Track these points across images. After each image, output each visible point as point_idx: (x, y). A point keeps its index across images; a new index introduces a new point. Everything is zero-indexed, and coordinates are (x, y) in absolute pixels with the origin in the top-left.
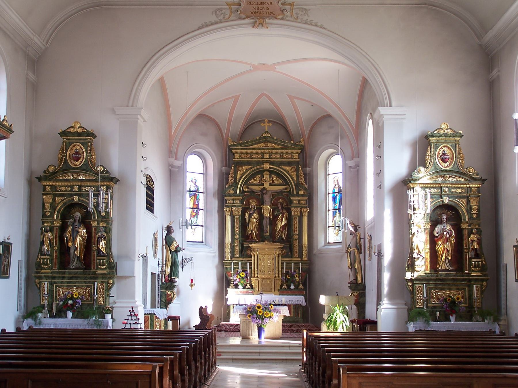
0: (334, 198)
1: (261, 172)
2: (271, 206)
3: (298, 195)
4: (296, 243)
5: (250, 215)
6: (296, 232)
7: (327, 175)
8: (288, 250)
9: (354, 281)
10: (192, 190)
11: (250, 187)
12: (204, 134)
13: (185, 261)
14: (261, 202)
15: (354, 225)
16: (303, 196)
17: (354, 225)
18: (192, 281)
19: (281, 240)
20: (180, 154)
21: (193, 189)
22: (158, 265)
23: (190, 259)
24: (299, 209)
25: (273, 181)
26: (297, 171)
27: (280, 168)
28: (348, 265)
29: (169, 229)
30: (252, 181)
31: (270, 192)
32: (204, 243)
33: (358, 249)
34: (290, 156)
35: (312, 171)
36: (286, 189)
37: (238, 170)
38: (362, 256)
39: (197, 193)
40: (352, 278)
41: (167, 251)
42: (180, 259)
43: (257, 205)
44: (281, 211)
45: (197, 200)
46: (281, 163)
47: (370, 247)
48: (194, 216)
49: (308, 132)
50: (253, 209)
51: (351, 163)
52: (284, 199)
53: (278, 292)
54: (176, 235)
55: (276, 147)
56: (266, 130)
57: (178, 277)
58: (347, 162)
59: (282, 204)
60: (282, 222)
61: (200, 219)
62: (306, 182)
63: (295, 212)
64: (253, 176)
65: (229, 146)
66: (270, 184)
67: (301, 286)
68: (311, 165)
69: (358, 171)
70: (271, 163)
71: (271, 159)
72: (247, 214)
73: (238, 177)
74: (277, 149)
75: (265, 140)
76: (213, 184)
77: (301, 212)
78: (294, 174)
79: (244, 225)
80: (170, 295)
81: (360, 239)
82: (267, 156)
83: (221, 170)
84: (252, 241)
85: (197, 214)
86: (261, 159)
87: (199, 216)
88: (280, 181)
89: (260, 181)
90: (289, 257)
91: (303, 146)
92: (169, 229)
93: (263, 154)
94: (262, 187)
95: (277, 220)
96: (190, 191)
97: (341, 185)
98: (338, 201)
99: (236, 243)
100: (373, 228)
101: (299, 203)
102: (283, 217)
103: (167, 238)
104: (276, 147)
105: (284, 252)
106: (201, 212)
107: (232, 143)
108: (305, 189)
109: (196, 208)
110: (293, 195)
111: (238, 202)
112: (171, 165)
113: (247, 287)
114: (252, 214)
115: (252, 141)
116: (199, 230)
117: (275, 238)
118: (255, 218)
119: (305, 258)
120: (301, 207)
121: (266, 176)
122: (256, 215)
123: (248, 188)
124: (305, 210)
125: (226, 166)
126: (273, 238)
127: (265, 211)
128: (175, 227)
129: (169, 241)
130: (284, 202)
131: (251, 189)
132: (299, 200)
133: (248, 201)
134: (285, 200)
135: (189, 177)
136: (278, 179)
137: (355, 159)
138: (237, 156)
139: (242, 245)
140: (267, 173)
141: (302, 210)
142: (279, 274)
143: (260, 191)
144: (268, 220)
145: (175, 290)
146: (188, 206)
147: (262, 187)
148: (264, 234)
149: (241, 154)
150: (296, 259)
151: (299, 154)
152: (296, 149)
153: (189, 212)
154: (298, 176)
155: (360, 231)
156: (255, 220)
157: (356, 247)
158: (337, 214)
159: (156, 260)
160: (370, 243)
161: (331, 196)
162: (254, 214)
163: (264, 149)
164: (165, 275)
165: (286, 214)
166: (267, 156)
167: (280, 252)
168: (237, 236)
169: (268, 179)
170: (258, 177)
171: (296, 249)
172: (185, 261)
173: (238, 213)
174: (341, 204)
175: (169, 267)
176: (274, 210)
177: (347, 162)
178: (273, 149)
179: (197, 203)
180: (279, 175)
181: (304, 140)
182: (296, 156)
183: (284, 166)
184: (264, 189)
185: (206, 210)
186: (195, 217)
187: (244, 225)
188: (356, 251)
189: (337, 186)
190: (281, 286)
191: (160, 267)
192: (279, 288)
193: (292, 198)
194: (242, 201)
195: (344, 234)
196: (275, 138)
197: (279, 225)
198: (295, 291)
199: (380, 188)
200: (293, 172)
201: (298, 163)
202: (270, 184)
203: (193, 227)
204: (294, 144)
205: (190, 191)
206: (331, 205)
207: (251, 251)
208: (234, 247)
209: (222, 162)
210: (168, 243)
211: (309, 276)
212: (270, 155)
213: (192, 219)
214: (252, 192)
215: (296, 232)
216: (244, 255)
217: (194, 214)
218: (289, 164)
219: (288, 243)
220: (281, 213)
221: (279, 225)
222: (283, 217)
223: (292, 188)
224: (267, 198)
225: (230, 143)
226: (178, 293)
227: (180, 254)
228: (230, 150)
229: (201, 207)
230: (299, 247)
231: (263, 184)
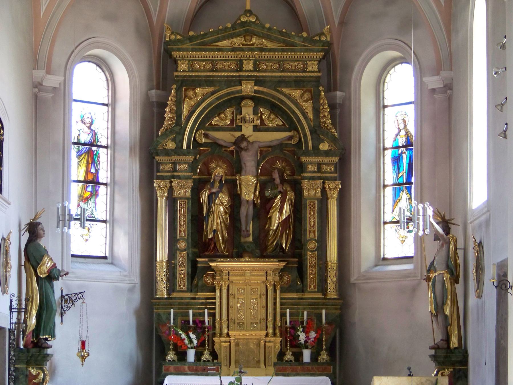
0: (397, 160)
1: (236, 102)
2: (257, 176)
3: (316, 151)
4: (311, 259)
5: (212, 197)
6: (312, 235)
7: (380, 107)
8: (295, 273)
9: (444, 345)
10: (82, 141)
11: (212, 134)
12: (111, 17)
13: (69, 300)
14: (236, 168)
15: (443, 218)
16: (327, 153)
17: (443, 218)
18: (83, 343)
19: (278, 253)
20: (58, 60)
21: (85, 138)
22: (11, 308)
23: (80, 296)
24: (319, 183)
25: (262, 121)
26: (315, 98)
27: (278, 91)
28: (430, 308)
29: (34, 230)
30: (215, 121)
31: (256, 146)
32: (109, 261)
33: (451, 273)
34: (300, 66)
35: (347, 99)
36: (291, 138)
37: (186, 96)
38: (459, 288)
39: (94, 148)
40: (439, 337)
41: (29, 277)
42: (57, 295)
43: (226, 175)
44: (280, 189)
45: (93, 162)
46: (279, 82)
47: (480, 269)
48: (87, 199)
49: (340, 11)
50: (217, 184)
51: (433, 82)
52: (286, 161)
53: (272, 369)
54: (48, 242)
55: (270, 45)
56: (248, 7)
57: (54, 336)
58: (424, 79)
59: (281, 173)
60: (280, 214)
61: (101, 207)
62: (334, 124)
63: (311, 190)
64: (217, 110)
65: (167, 43)
66: (256, 129)
67: (324, 356)
68: (345, 86)
69: (450, 99)
70: (258, 82)
71: (259, 71)
72: (205, 196)
73: (185, 112)
74: (270, 50)
75: (246, 30)
76: (127, 124)
77: (324, 190)
78: (308, 106)
79: (198, 219)
80: (36, 377)
81: (456, 249)
82: (249, 66)
83: (147, 97)
84: (217, 256)
85: (95, 194)
86: (237, 71)
87: (98, 200)
88: (278, 122)
89: (233, 121)
90: (297, 291)
91: (329, 44)
92: (34, 230)
93: (241, 61)
94: (238, 134)
95: (271, 207)
96: (78, 143)
97: (412, 128)
98: (405, 166)
99: (181, 258)
100: (487, 223)
101: (319, 170)
102: (283, 202)
103: (31, 249)
104: (270, 45)
105: (285, 279)
106: (102, 190)
107: (173, 37)
108: (333, 140)
109: (92, 181)
110: (307, 153)
111: (185, 167)
112: (38, 86)
113: (203, 358)
114: (216, 194)
115: (218, 32)
116: (99, 231)
117: (266, 247)
118: (222, 204)
119: (332, 292)
120: (325, 180)
121: (248, 110)
122: (224, 198)
123: (206, 136)
124: (332, 185)
125: (158, 88)
126: (261, 250)
127: (243, 188)
128: (48, 224)
129: (33, 255)
130: (285, 169)
131: (214, 139)
132: (319, 165)
133: (206, 165)
134: (289, 164)
135: (77, 111)
136: (272, 116)
137: (444, 74)
138: (183, 66)
139: (194, 265)
140: (250, 102)
141: (327, 185)
142: (274, 328)
143: (235, 143)
144: (251, 208)
145: (47, 367)
146: (74, 177)
147: (238, 134)
148: (243, 240)
149: (191, 61)
150: (312, 294)
151: (319, 61)
152: (313, 51)
153: (76, 189)
154: (317, 111)
155: (457, 231)
156: (222, 209)
157: (448, 267)
158: (404, 196)
159: (7, 298)
160: (479, 259)
161: (389, 155)
162: (221, 195)
163: (242, 50)
164: (24, 332)
165: (291, 195)
166: (249, 66)
167: (277, 278)
168: (182, 245)
169: (252, 117)
170: (229, 112)
171: (312, 274)
172: (69, 300)
173: (183, 191)
174: (410, 174)
175: (34, 313)
176: (264, 185)
177: (424, 79)
178: (262, 50)
179: (93, 170)
180: (276, 109)
181: (330, 31)
182: (313, 66)
183: (286, 87)
184: (243, 138)
185: (113, 184)
186: (90, 202)
187: (198, 219)
188: (447, 276)
189: (403, 133)
190: (281, 355)
191: (15, 315)
192: (274, 359)
193: (304, 159)
194: (192, 167)
195: (419, 241)
196: (267, 26)
197: (276, 219)
198: (310, 367)
199: (505, 137)
200: (306, 101)
201: (317, 81)
202: (256, 129)
203: (87, 223)
204: (310, 40)
205: (78, 143)
206: (390, 176)
207: (213, 277)
208: (175, 268)
209: (149, 79)
210: (32, 259)
211: (341, 334)
212: (255, 64)
213: (82, 204)
214: (216, 145)
215: (312, 235)
216: (197, 285)
217: (87, 194)
218: (298, 83)
219: (294, 256)
220: (280, 192)
221: (276, 219)
222: (283, 202)
223: (305, 135)
224: (249, 161)
225: (169, 36)
226: (53, 372)
227: (58, 285)
228: (168, 53)
229: (103, 177)
230: (320, 269)
231: (239, 129)
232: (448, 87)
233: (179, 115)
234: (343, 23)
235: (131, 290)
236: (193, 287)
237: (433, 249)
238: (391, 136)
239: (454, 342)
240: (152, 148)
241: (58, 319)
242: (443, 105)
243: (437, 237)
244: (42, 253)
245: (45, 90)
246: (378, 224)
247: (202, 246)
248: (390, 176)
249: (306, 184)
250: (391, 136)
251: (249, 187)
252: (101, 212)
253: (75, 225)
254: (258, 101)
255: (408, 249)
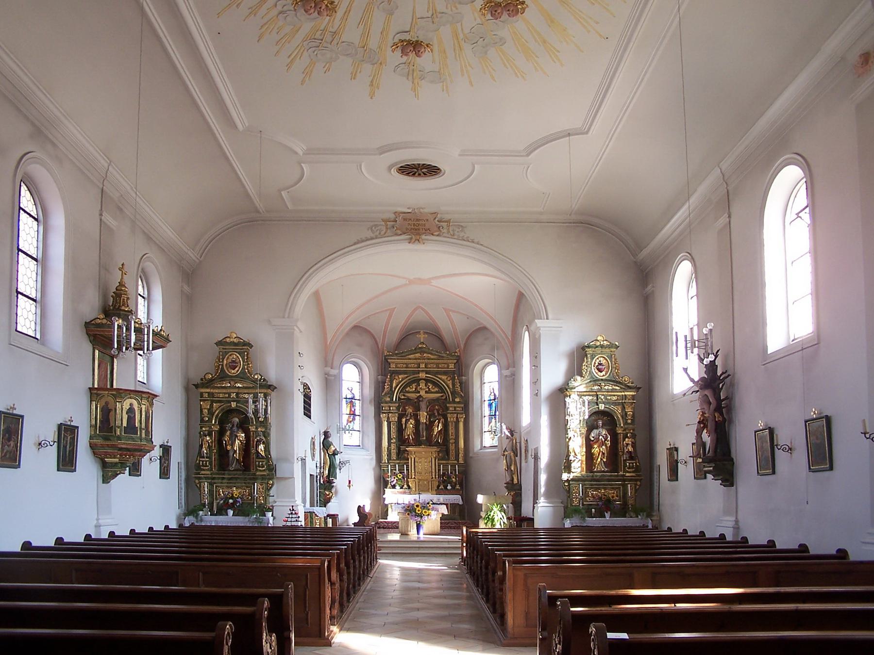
0: (490, 405)
1: (417, 381)
3: (454, 402)
4: (452, 447)
5: (407, 421)
7: (482, 383)
12: (360, 345)
14: (418, 409)
16: (459, 403)
19: (437, 444)
20: (336, 363)
21: (350, 396)
26: (453, 379)
28: (505, 467)
29: (326, 434)
38: (518, 459)
41: (325, 454)
42: (338, 462)
47: (526, 451)
51: (506, 372)
55: (432, 357)
60: (438, 428)
61: (357, 424)
63: (451, 418)
64: (409, 384)
66: (426, 392)
72: (404, 420)
73: (394, 385)
75: (422, 351)
76: (369, 392)
78: (450, 383)
85: (354, 419)
88: (436, 389)
92: (326, 434)
98: (494, 408)
99: (393, 446)
104: (432, 357)
106: (357, 418)
109: (353, 414)
110: (450, 403)
119: (461, 461)
121: (422, 385)
126: (429, 442)
129: (326, 445)
130: (439, 409)
133: (404, 407)
135: (345, 385)
137: (511, 369)
139: (399, 449)
145: (333, 490)
154: (454, 385)
158: (493, 420)
161: (487, 403)
165: (442, 420)
170: (414, 385)
173: (394, 418)
180: (435, 384)
182: (452, 366)
187: (400, 430)
190: (438, 486)
194: (398, 408)
195: (500, 439)
202: (426, 392)
204: (450, 355)
206: (486, 411)
209: (378, 372)
214: (409, 399)
218: (445, 373)
219: (445, 447)
224: (423, 405)
226: (336, 492)
228: (386, 360)
229: (357, 413)
232: (513, 375)
233: (392, 387)
234: (465, 344)
235: (371, 459)
236: (398, 458)
237: (506, 443)
238: (487, 396)
239: (515, 481)
240: (379, 401)
241: (338, 470)
242: (510, 383)
243: (508, 437)
244: (330, 444)
245: (331, 376)
246: (481, 433)
247: (402, 441)
248: (486, 411)
249: (449, 415)
250: (487, 396)
251: (423, 417)
252: (357, 427)
253: (100, 521)
254: (427, 381)
255: (495, 443)
